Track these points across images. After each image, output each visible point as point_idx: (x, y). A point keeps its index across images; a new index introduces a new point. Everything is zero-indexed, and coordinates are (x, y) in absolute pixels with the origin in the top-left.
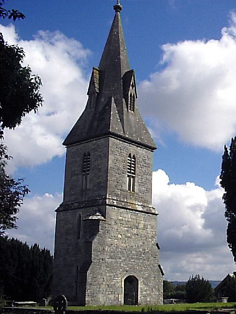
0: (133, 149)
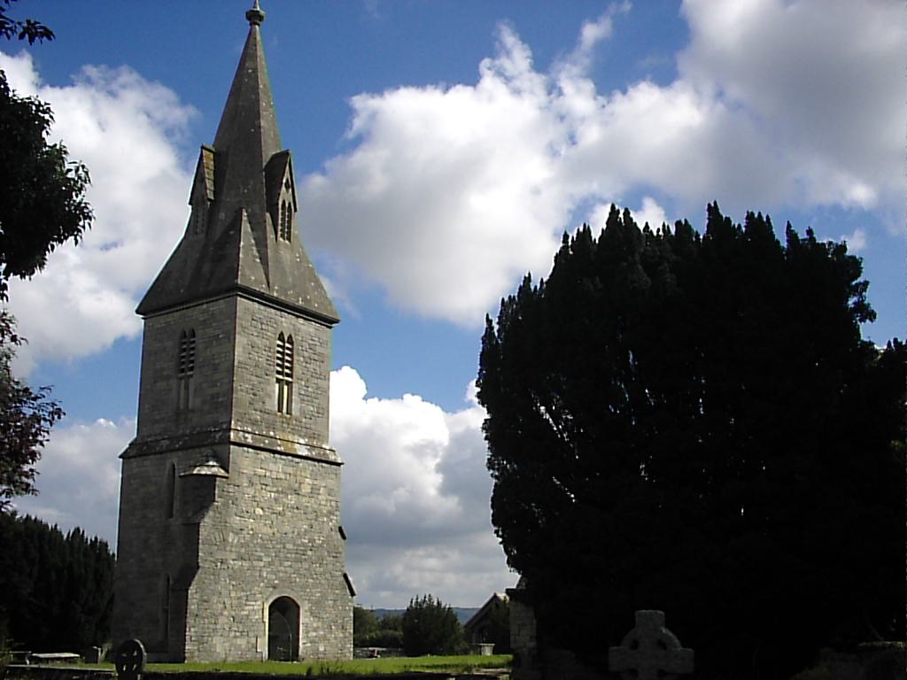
0: (287, 322)
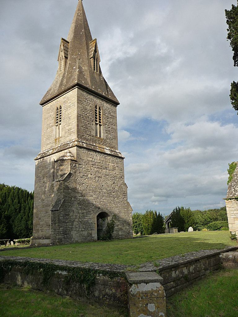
0: (98, 102)
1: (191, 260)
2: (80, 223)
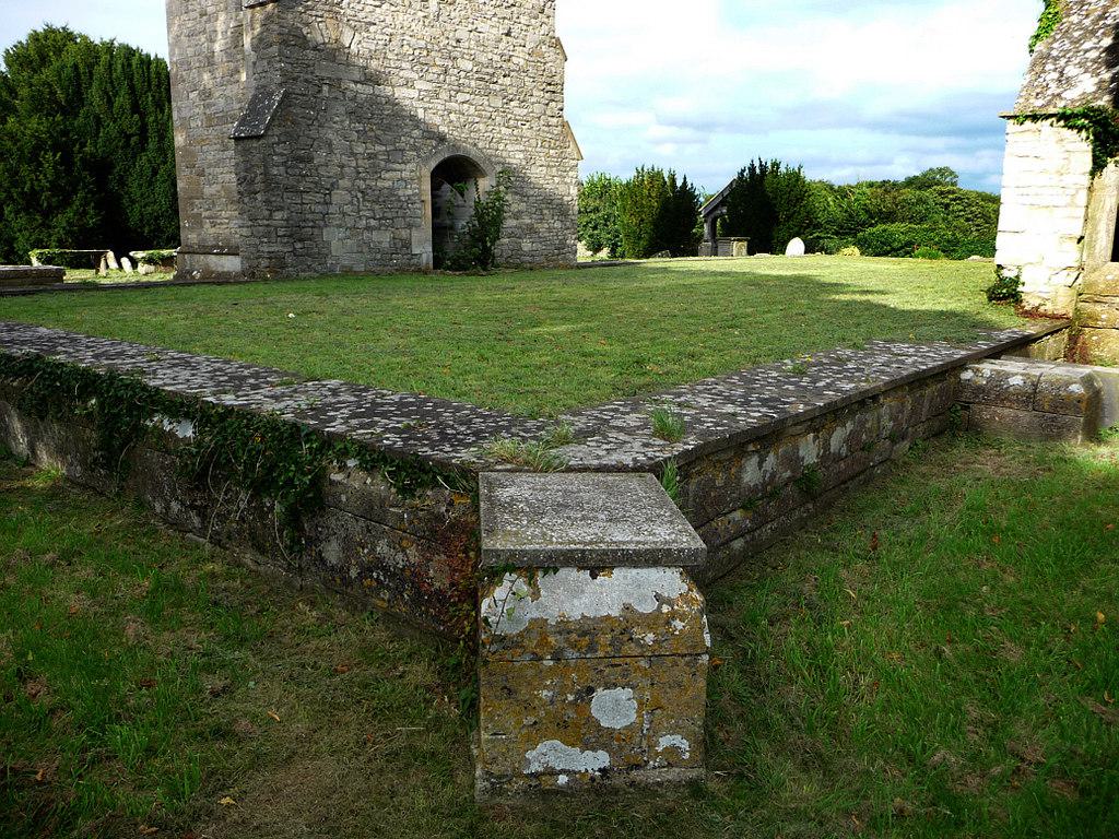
1: (843, 399)
2: (360, 195)
